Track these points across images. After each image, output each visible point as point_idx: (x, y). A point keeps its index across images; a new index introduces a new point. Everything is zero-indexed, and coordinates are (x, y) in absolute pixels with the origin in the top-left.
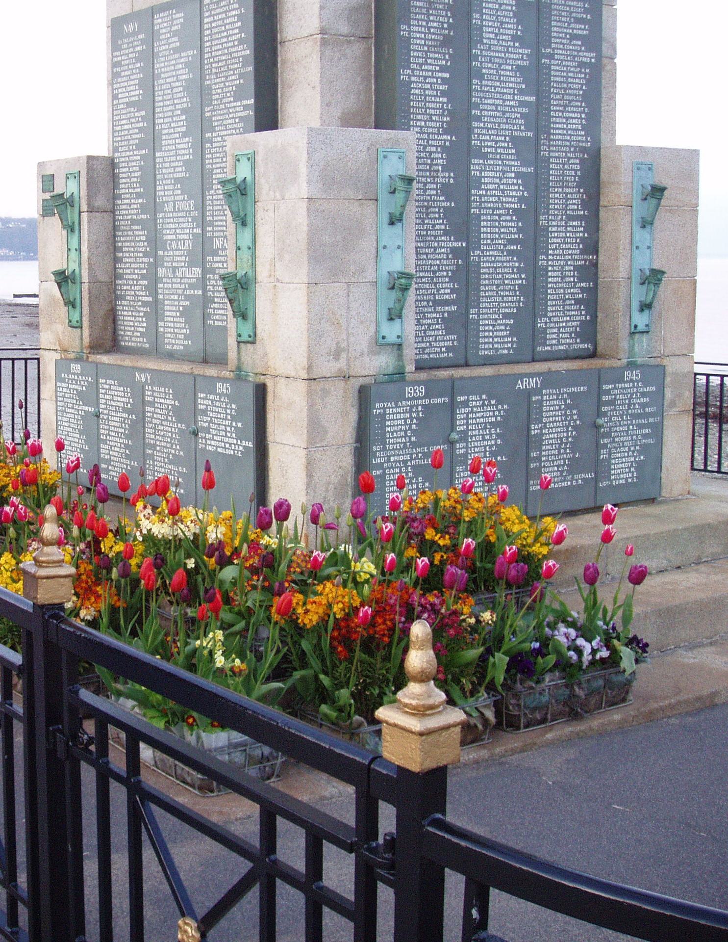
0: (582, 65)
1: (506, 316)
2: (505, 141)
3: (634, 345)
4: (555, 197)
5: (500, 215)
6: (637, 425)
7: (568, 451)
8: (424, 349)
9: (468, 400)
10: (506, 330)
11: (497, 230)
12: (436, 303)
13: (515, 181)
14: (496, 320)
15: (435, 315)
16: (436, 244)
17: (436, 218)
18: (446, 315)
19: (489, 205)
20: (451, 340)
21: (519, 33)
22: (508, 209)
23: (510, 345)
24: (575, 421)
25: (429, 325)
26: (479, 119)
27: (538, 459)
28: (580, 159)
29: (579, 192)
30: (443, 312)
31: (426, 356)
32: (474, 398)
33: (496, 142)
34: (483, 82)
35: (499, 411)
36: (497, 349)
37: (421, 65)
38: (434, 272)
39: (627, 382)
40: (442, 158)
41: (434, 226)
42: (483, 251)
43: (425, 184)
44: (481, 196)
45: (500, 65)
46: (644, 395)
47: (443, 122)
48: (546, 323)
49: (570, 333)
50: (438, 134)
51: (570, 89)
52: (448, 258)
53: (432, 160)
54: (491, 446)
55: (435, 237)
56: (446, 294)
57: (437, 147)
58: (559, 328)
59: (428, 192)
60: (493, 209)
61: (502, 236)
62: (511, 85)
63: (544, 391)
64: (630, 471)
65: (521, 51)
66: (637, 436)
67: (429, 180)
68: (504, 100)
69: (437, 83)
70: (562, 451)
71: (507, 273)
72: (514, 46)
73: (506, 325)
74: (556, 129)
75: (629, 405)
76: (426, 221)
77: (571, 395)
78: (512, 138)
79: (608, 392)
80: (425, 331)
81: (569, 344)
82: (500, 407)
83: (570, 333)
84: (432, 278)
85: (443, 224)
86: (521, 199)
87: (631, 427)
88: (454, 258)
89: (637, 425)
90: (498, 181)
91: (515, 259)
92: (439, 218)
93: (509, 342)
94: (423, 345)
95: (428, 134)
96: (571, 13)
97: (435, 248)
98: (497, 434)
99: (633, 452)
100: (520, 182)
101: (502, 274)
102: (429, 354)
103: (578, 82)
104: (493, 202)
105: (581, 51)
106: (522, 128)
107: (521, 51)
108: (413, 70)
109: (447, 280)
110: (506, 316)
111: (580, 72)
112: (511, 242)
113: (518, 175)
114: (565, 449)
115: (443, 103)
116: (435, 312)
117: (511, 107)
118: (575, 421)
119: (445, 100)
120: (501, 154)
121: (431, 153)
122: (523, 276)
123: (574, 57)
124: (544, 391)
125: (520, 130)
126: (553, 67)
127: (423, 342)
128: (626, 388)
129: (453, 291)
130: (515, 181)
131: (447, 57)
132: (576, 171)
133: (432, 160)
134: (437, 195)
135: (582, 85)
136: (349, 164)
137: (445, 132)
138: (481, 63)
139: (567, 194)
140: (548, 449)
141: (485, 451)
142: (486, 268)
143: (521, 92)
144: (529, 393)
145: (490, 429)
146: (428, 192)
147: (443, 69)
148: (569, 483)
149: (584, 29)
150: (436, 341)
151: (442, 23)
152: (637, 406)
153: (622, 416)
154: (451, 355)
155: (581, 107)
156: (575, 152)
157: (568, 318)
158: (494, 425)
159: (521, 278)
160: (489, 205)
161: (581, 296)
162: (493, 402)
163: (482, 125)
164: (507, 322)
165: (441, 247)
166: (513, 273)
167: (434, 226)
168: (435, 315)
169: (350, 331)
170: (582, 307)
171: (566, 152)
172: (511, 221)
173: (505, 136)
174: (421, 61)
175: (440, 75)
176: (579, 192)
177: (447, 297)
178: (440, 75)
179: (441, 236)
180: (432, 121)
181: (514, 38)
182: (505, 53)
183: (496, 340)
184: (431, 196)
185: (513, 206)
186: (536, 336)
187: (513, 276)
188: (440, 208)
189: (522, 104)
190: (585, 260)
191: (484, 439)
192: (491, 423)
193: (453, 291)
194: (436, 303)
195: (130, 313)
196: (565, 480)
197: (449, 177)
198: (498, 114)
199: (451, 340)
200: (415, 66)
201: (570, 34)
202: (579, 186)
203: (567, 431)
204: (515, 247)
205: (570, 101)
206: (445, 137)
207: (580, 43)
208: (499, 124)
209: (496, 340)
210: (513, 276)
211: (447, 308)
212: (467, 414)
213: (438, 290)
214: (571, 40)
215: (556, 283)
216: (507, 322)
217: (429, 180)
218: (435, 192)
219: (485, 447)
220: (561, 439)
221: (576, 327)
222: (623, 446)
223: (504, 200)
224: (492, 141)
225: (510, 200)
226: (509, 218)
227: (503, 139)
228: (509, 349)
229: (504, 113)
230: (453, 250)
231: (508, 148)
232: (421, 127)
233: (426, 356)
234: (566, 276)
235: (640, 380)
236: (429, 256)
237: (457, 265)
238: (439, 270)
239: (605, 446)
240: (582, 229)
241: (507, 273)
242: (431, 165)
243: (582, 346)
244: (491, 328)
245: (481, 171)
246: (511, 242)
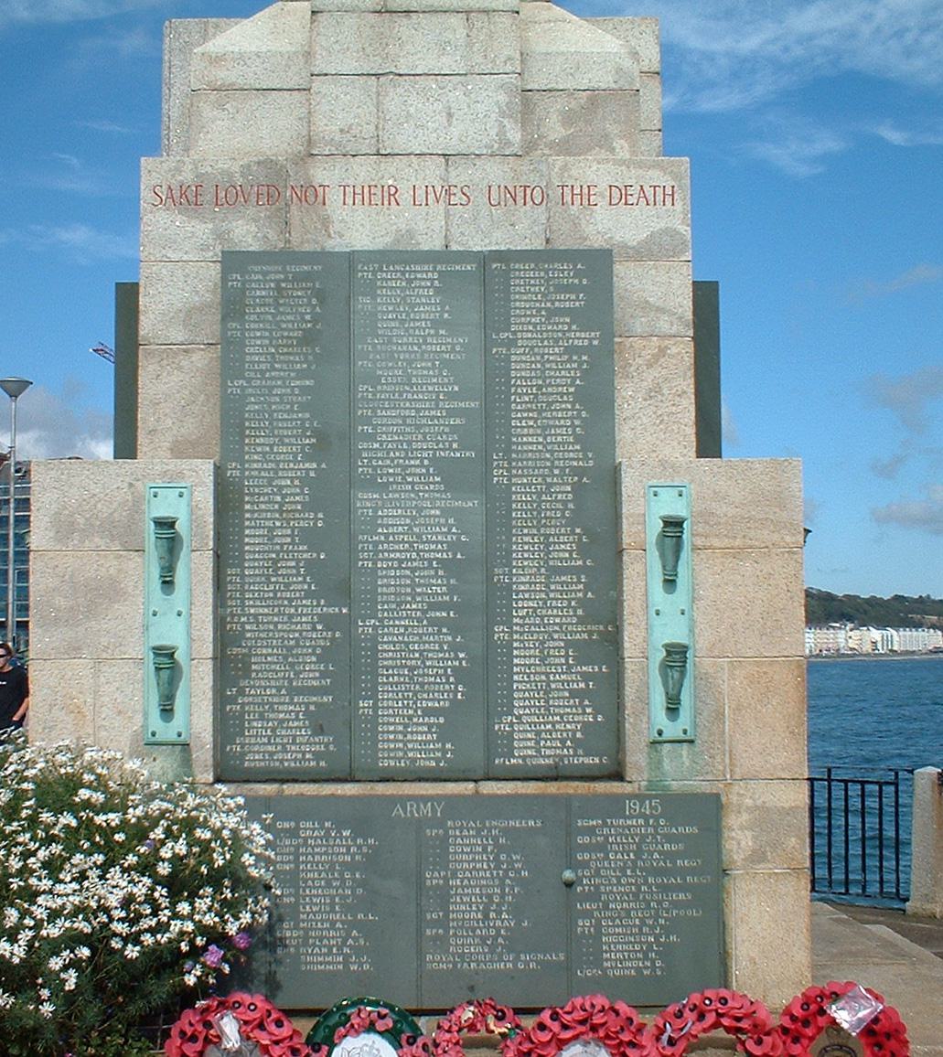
0: (570, 350)
1: (428, 712)
2: (422, 466)
3: (660, 762)
4: (524, 547)
5: (413, 570)
6: (658, 886)
7: (505, 916)
8: (272, 754)
9: (298, 828)
10: (430, 732)
11: (409, 590)
12: (292, 691)
13: (442, 521)
14: (410, 718)
15: (291, 708)
16: (293, 610)
17: (293, 575)
18: (312, 708)
19: (392, 556)
20: (322, 743)
21: (446, 315)
22: (430, 561)
23: (439, 754)
24: (518, 871)
25: (282, 721)
26: (371, 438)
27: (443, 923)
28: (573, 485)
29: (573, 533)
30: (307, 705)
31: (277, 764)
32: (309, 825)
33: (405, 468)
34: (379, 388)
35: (359, 847)
36: (414, 760)
37: (263, 372)
38: (290, 649)
39: (631, 817)
40: (302, 493)
41: (287, 585)
42: (381, 620)
43: (271, 529)
44: (376, 544)
45: (410, 362)
46: (670, 838)
47: (303, 446)
48: (511, 725)
49: (563, 741)
50: (295, 461)
51: (550, 385)
52: (314, 629)
53: (284, 496)
54: (343, 897)
55: (290, 600)
56: (311, 674)
57: (292, 479)
58: (538, 733)
59: (277, 540)
60: (400, 561)
61: (419, 599)
62: (430, 389)
63: (450, 823)
64: (646, 958)
65: (449, 340)
66: (659, 903)
67: (278, 524)
68: (418, 410)
69: (293, 394)
70: (492, 915)
71: (430, 651)
72: (437, 335)
73: (430, 726)
74: (523, 444)
75: (639, 853)
76: (273, 579)
77: (506, 831)
78: (433, 460)
79: (591, 831)
80: (273, 730)
81: (562, 757)
82: (359, 841)
83: (563, 741)
84: (285, 657)
85: (304, 582)
86: (453, 546)
87: (644, 888)
88: (327, 628)
89: (658, 886)
90: (408, 521)
91: (444, 630)
92: (298, 574)
93: (438, 750)
94: (270, 748)
95: (277, 462)
96: (549, 279)
97: (291, 616)
98: (354, 880)
99: (652, 928)
100: (451, 521)
101: (421, 652)
102: (281, 761)
103: (565, 377)
104: (400, 551)
105: (569, 330)
106: (455, 446)
107: (449, 340)
108: (249, 380)
109: (314, 659)
110: (428, 712)
111: (570, 361)
112: (434, 606)
113: (446, 512)
114: (499, 913)
115: (303, 420)
116: (291, 703)
117: (432, 418)
118: (518, 871)
119: (307, 415)
120: (413, 483)
121: (281, 488)
122: (462, 655)
123: (556, 340)
124: (450, 823)
125: (450, 448)
126: (513, 358)
127: (269, 743)
128: (629, 827)
129: (324, 675)
130: (442, 521)
131: (310, 358)
132: (565, 503)
133: (284, 496)
134: (293, 543)
135: (574, 379)
136: (99, 506)
137: (308, 458)
138: (374, 361)
139: (547, 536)
140: (465, 908)
141: (333, 904)
142: (389, 642)
143: (451, 396)
144: (420, 824)
145: (341, 874)
146: (277, 540)
147: (301, 375)
148: (510, 965)
149: (577, 299)
150: (294, 743)
151: (302, 314)
152: (656, 856)
153: (623, 870)
154: (322, 764)
155: (572, 410)
156: (561, 476)
157: (558, 718)
158: (351, 866)
159: (457, 658)
160: (392, 556)
161: (582, 685)
162: (346, 833)
163: (376, 445)
164: (432, 720)
165: (302, 615)
166: (442, 650)
167: (287, 585)
168: (291, 708)
169: (99, 722)
170: (587, 702)
171: (544, 476)
172: (436, 576)
173: (422, 459)
174: (263, 367)
175: (298, 383)
176: (573, 533)
177: (315, 683)
178: (298, 383)
179: (301, 599)
180: (283, 444)
181: (436, 324)
182: (419, 346)
183: (410, 746)
184: (282, 545)
185: (439, 556)
186: (496, 743)
187: (441, 655)
188: (298, 561)
189: (451, 413)
190: (590, 633)
191: (329, 885)
192: (343, 864)
193: (324, 675)
194: (292, 691)
195: (527, 711)
196: (501, 960)
197: (316, 519)
198: (408, 430)
199: (322, 743)
200: (252, 374)
201: (547, 309)
202: (572, 523)
203: (502, 886)
204: (444, 614)
205: (550, 404)
206: (307, 465)
207: (568, 320)
208: (409, 443)
209: (410, 746)
210: (441, 655)
211: (315, 699)
212: (297, 848)
213: (297, 674)
214: (548, 318)
215: (529, 666)
216: (432, 720)
217: (278, 524)
218: (289, 540)
219: (332, 898)
220: (490, 897)
221: (574, 732)
222: (629, 916)
223: (421, 547)
224: (398, 466)
225: (433, 547)
226: (432, 573)
227: (418, 462)
228: (438, 760)
229: (418, 427)
230: (323, 618)
231: (428, 474)
232: (264, 454)
233: (277, 764)
234: (549, 656)
235: (661, 816)
236: (280, 626)
237: (333, 639)
238: (297, 646)
239: (587, 914)
240: (581, 586)
241: (430, 651)
242: (281, 505)
243: (588, 761)
244: (401, 728)
245: (375, 510)
246: (434, 606)
